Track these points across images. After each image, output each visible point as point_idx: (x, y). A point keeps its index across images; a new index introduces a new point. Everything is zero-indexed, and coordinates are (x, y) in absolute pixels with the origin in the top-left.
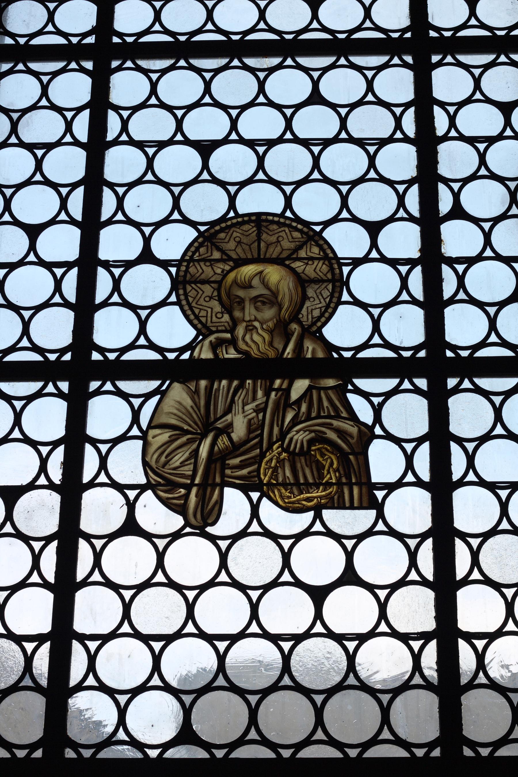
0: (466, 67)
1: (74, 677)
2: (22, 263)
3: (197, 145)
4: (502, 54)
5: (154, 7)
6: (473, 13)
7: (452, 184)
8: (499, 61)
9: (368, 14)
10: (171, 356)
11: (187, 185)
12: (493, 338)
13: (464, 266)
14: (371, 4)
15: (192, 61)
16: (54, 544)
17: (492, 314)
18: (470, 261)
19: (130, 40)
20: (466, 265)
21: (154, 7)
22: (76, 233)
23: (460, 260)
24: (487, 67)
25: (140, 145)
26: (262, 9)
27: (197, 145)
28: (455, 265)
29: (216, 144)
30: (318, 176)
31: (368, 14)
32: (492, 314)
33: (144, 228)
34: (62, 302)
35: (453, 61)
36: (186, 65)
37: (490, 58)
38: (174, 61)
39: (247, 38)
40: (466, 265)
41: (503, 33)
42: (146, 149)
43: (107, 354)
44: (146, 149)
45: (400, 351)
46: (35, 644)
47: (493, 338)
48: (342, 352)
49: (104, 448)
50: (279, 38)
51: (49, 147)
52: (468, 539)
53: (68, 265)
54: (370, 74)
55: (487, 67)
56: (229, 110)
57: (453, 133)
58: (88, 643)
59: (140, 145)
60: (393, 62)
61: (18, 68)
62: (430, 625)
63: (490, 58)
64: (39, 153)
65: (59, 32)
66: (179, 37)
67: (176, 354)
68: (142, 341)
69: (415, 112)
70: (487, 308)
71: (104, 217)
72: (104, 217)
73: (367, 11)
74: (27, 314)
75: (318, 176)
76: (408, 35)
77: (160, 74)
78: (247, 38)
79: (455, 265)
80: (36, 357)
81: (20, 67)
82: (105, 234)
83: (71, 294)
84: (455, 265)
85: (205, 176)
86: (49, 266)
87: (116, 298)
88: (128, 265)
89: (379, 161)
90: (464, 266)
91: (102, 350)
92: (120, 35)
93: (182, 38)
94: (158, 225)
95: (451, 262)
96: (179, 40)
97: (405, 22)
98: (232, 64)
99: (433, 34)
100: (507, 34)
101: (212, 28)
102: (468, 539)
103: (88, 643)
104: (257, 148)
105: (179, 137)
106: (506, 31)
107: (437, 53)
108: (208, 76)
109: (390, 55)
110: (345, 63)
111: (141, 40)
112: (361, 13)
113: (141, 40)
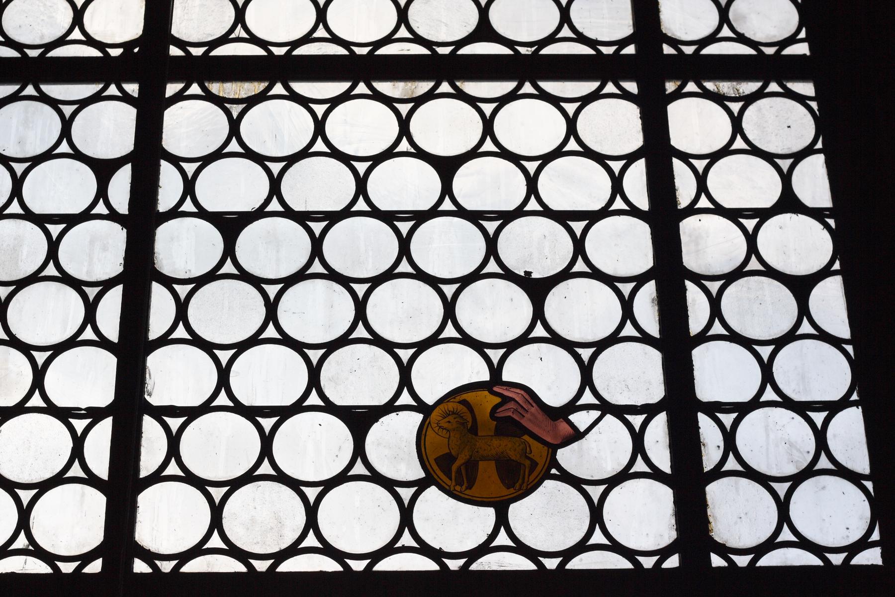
0: (472, 101)
3: (218, 219)
4: (30, 83)
6: (724, 18)
7: (707, 283)
8: (24, 93)
9: (78, 20)
12: (407, 539)
13: (824, 414)
14: (85, 6)
15: (790, 85)
17: (596, 499)
18: (743, 409)
19: (197, 52)
20: (644, 416)
22: (109, 361)
23: (174, 411)
24: (586, 100)
26: (564, 6)
27: (218, 219)
28: (259, 419)
29: (245, 218)
31: (78, 20)
32: (596, 499)
33: (35, 354)
34: (823, 453)
35: (451, 91)
36: (451, 91)
37: (592, 86)
38: (102, 85)
39: (215, 53)
40: (644, 416)
41: (364, 51)
43: (446, 561)
45: (80, 562)
47: (407, 539)
48: (59, 564)
50: (19, 55)
51: (333, 218)
53: (95, 415)
54: (488, 108)
55: (586, 100)
57: (704, 203)
60: (24, 93)
61: (606, 90)
63: (592, 86)
64: (55, 230)
65: (90, 41)
66: (109, 50)
67: (461, 562)
68: (216, 541)
69: (819, 566)
70: (398, 490)
71: (154, 333)
72: (154, 333)
73: (484, 12)
74: (26, 496)
76: (630, 50)
77: (329, 105)
78: (215, 53)
79: (258, 419)
81: (278, 89)
82: (155, 361)
83: (100, 465)
84: (258, 419)
86: (64, 415)
87: (173, 469)
89: (328, 248)
90: (824, 414)
92: (182, 44)
93: (33, 53)
94: (242, 347)
95: (713, 409)
96: (436, 52)
97: (624, 27)
98: (24, 93)
99: (667, 50)
100: (371, 52)
101: (408, 35)
104: (398, 224)
105: (447, 205)
106: (451, 48)
107: (672, 78)
108: (570, 108)
109: (681, 81)
110: (34, 93)
111: (214, 53)
112: (555, 16)
113: (214, 53)
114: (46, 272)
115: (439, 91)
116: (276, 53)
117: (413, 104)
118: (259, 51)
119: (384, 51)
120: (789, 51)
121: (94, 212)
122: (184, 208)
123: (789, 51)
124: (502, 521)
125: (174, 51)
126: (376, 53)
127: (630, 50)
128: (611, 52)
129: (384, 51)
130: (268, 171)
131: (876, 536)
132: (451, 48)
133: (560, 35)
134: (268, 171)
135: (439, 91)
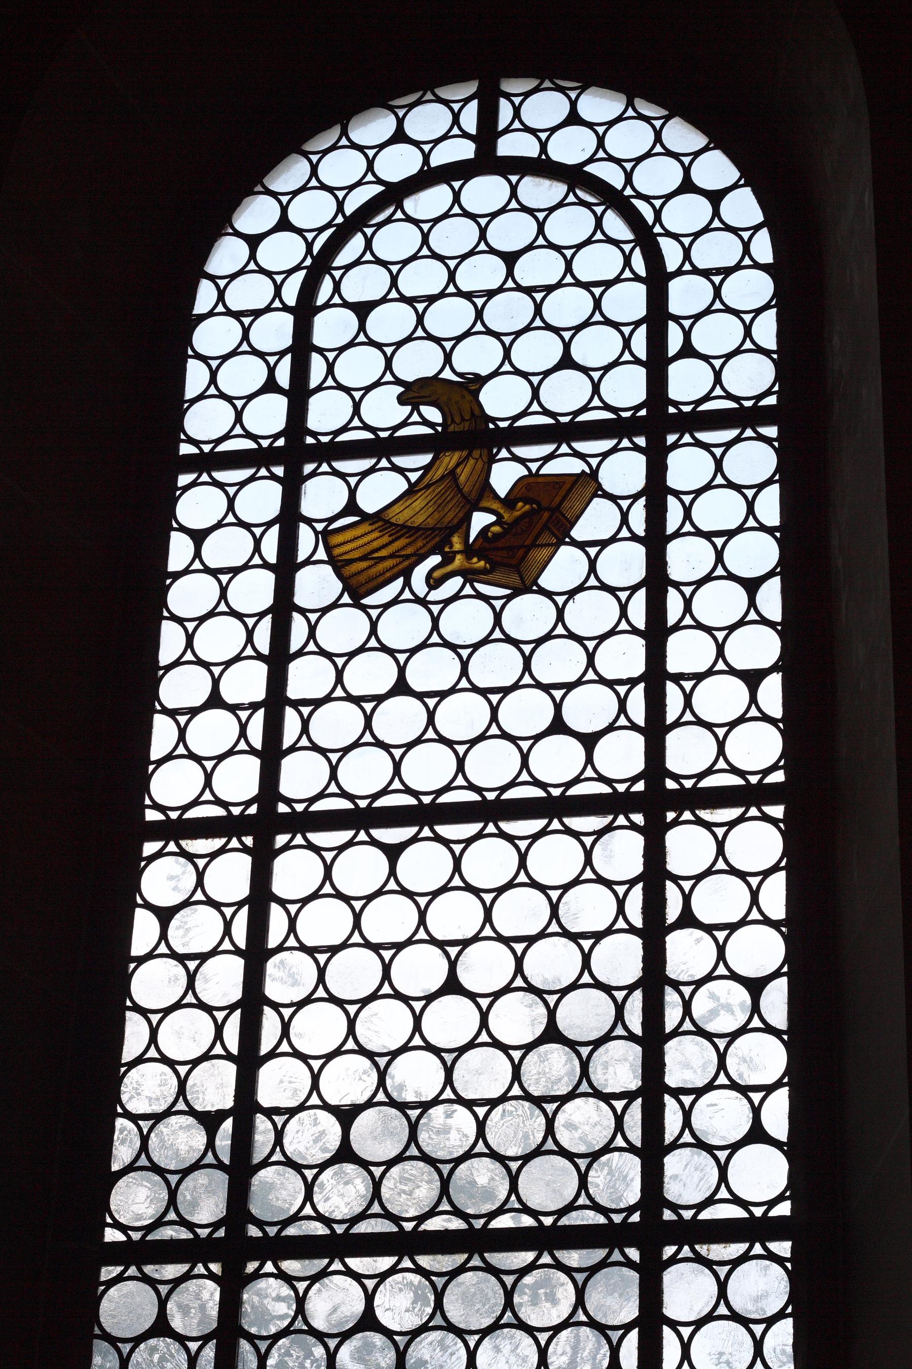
1: (633, 1299)
2: (710, 672)
5: (509, 182)
10: (748, 404)
11: (639, 160)
15: (552, 421)
16: (642, 501)
21: (509, 182)
23: (305, 702)
25: (468, 296)
30: (743, 234)
42: (475, 299)
44: (475, 299)
46: (525, 944)
49: (686, 1332)
52: (200, 800)
56: (563, 251)
58: (751, 1094)
59: (468, 296)
62: (634, 1083)
75: (743, 234)
76: (643, 412)
78: (518, 424)
80: (368, 435)
85: (507, 340)
88: (193, 712)
91: (288, 802)
100: (755, 404)
102: (200, 800)
103: (751, 1094)
114: (570, 333)
115: (759, 776)
116: (381, 436)
117: (344, 1005)
118: (550, 421)
119: (521, 423)
120: (764, 403)
121: (249, 350)
122: (445, 1173)
123: (764, 403)
124: (426, 157)
125: (310, 440)
126: (759, 405)
127: (643, 412)
128: (327, 441)
129: (521, 423)
130: (605, 151)
131: (776, 388)
132: (753, 401)
133: (340, 144)
134: (605, 151)
135: (759, 776)
